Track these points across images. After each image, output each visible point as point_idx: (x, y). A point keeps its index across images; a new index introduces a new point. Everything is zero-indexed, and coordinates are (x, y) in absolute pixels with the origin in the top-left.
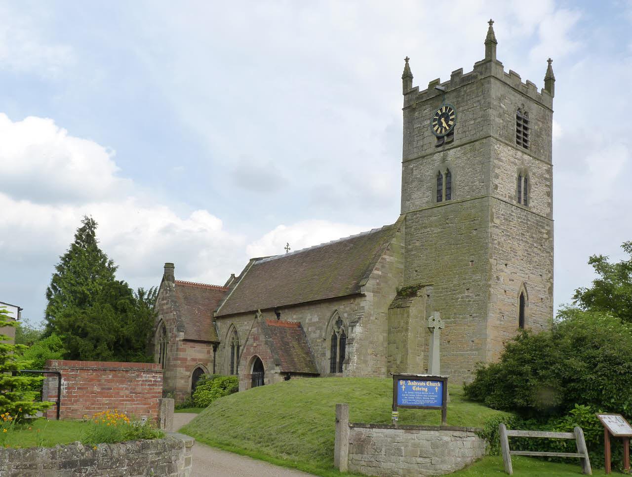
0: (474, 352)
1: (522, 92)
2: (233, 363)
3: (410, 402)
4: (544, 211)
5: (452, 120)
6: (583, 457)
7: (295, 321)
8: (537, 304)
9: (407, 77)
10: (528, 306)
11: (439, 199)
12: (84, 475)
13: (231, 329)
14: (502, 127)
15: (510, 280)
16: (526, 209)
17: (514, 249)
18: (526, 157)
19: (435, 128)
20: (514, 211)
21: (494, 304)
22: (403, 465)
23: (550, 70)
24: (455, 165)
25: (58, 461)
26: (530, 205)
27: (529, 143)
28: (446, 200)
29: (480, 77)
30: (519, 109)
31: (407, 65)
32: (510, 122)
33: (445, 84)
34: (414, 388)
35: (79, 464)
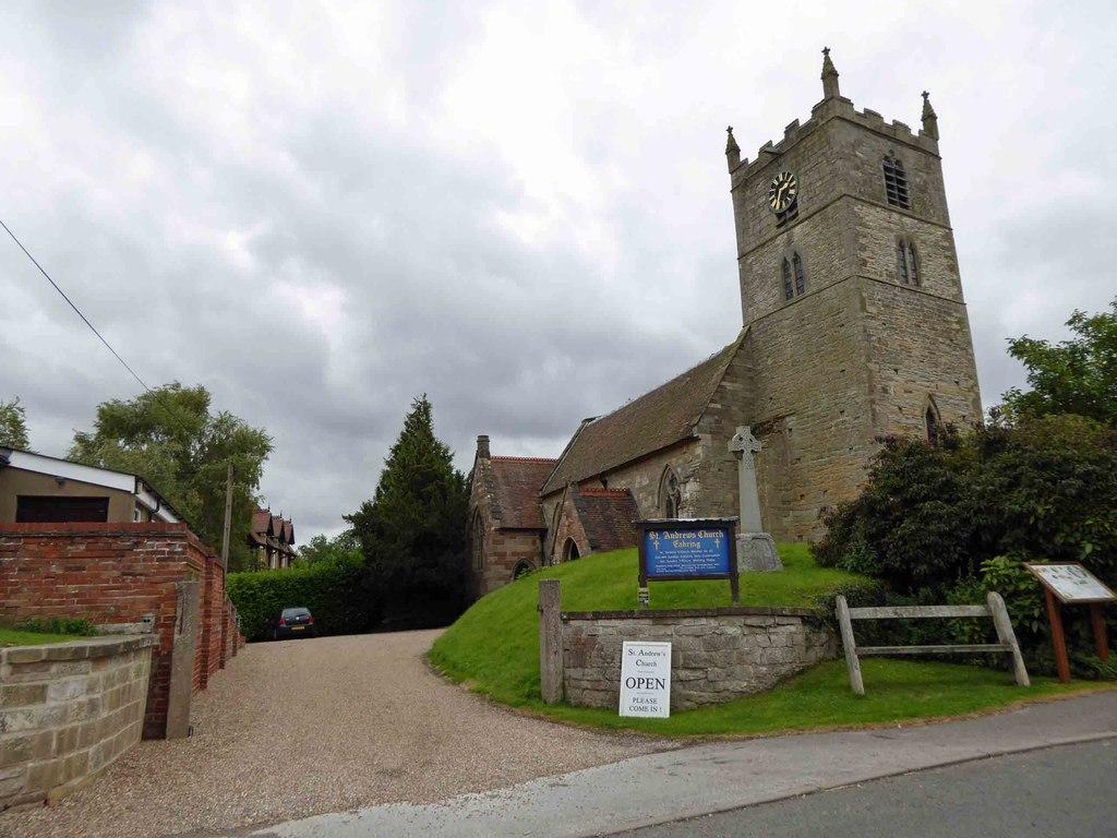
4: (949, 293)
6: (1008, 650)
9: (733, 150)
11: (789, 295)
15: (906, 392)
18: (905, 219)
19: (773, 205)
23: (927, 106)
31: (731, 136)
33: (780, 145)
34: (675, 544)
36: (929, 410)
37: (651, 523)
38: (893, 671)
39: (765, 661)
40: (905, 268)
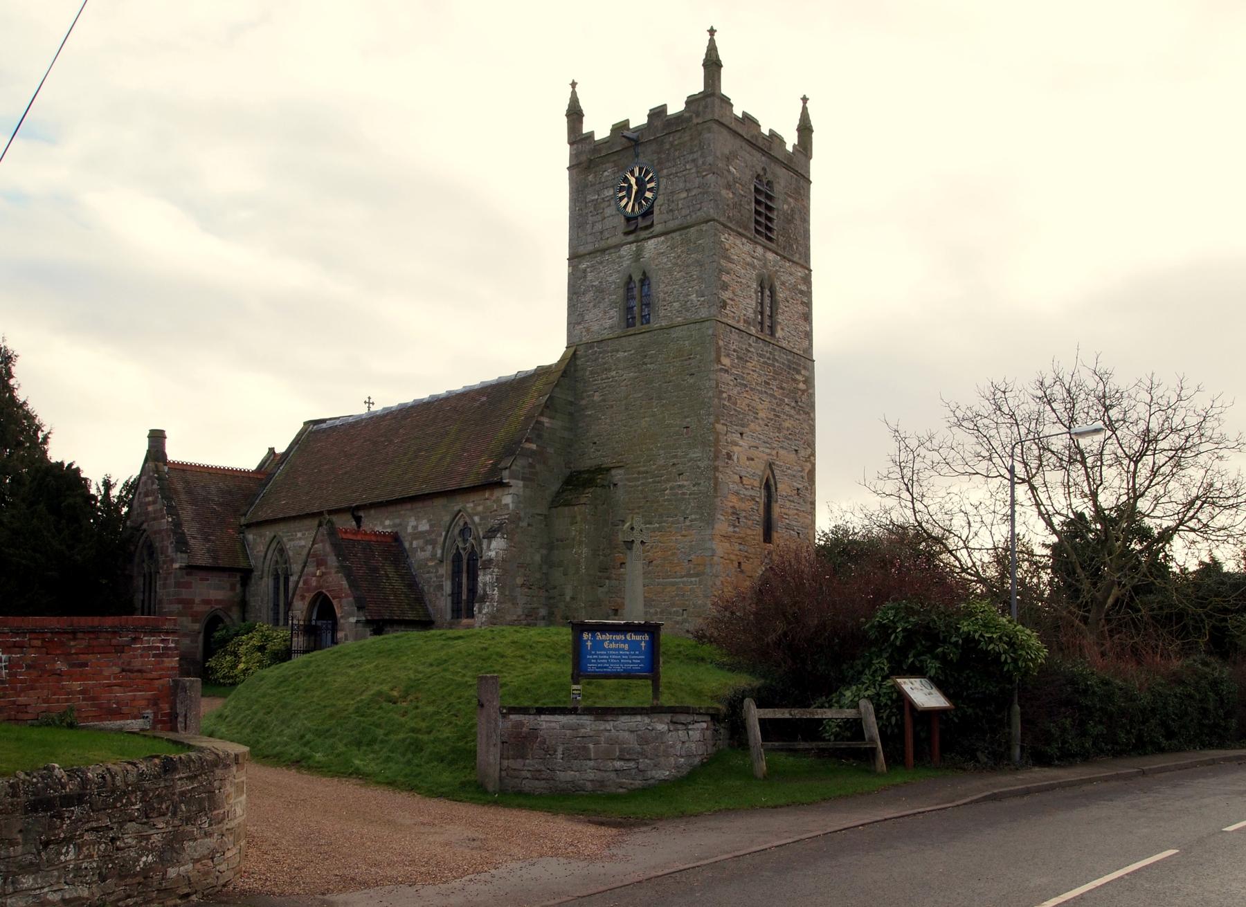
0: (693, 579)
1: (763, 148)
2: (276, 605)
3: (600, 667)
5: (651, 190)
7: (389, 530)
8: (791, 499)
9: (575, 114)
10: (777, 501)
12: (69, 821)
13: (274, 545)
14: (732, 205)
16: (772, 342)
17: (753, 408)
18: (770, 256)
20: (753, 344)
21: (723, 499)
22: (591, 775)
24: (657, 265)
25: (23, 799)
26: (777, 335)
27: (775, 233)
28: (642, 324)
29: (695, 121)
30: (758, 175)
32: (745, 197)
33: (638, 129)
35: (59, 803)
36: (767, 480)
37: (587, 624)
38: (785, 761)
39: (683, 753)
40: (762, 313)
